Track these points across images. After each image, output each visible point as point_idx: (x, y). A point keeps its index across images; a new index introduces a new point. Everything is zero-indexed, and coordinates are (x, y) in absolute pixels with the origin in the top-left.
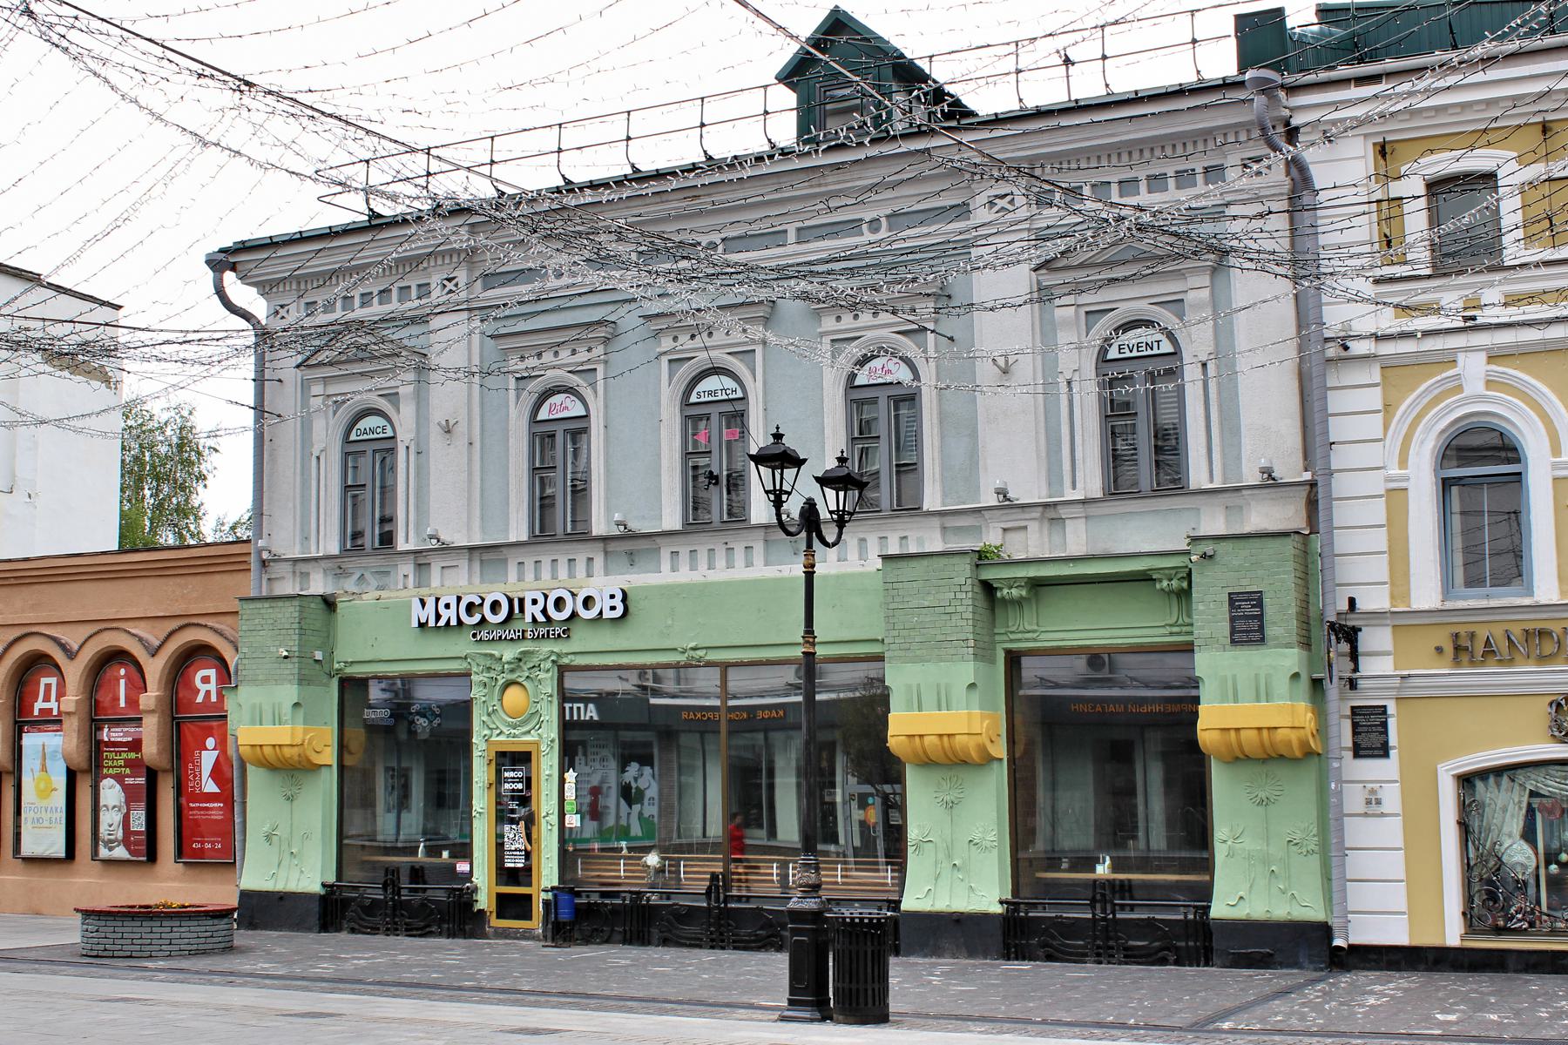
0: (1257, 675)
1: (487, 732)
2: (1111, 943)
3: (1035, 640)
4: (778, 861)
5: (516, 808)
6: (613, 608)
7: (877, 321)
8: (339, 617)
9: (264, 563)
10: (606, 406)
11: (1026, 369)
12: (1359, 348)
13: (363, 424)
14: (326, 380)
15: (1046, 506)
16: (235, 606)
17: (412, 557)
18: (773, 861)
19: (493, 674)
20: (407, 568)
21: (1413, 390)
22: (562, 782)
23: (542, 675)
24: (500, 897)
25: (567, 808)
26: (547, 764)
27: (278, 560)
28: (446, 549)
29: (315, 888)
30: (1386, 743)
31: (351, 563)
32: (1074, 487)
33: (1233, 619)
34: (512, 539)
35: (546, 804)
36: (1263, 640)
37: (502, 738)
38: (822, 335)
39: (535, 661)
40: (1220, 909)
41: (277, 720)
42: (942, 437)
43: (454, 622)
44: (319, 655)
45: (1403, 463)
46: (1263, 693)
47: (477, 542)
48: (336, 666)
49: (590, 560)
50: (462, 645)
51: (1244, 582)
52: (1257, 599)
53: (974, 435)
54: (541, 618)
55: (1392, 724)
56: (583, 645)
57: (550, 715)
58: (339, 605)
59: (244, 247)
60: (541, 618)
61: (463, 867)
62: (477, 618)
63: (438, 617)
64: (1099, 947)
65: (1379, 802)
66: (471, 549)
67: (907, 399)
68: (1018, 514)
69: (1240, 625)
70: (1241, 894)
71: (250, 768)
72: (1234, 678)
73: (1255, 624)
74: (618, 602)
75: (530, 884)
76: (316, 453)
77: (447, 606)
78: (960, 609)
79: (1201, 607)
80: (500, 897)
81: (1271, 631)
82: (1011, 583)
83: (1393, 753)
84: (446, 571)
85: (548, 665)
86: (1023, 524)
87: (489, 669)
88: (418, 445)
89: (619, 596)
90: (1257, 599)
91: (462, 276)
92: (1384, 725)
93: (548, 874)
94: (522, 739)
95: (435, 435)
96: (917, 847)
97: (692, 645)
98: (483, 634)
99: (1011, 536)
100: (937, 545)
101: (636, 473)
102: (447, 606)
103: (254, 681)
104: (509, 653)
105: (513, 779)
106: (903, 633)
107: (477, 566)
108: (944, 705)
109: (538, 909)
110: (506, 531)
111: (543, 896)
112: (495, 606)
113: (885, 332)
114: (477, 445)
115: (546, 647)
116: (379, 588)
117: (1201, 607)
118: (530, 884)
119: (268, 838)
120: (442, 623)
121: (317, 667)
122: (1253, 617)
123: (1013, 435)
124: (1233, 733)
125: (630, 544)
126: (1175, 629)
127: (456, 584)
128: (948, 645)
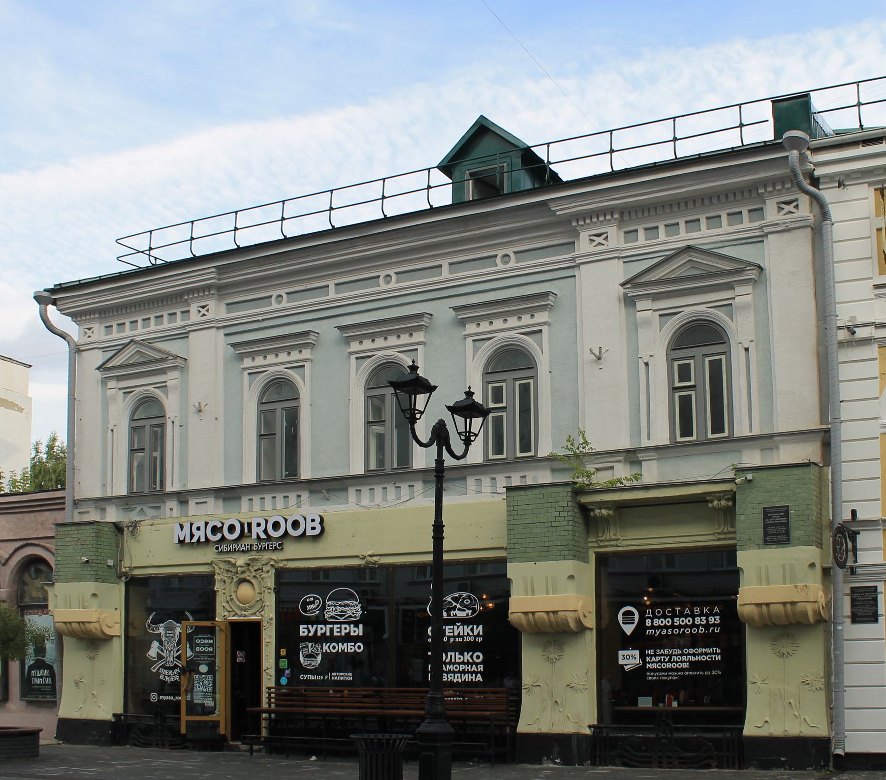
6: (313, 528)
12: (861, 333)
14: (119, 378)
19: (230, 574)
20: (173, 504)
23: (264, 575)
29: (109, 717)
30: (876, 612)
32: (649, 439)
33: (766, 526)
34: (353, 472)
36: (788, 540)
38: (466, 337)
39: (258, 565)
43: (203, 539)
47: (221, 483)
48: (124, 570)
51: (775, 499)
54: (263, 536)
56: (297, 555)
57: (270, 600)
60: (263, 536)
62: (219, 536)
63: (192, 536)
70: (767, 719)
72: (767, 567)
73: (783, 529)
76: (110, 428)
79: (742, 518)
81: (795, 534)
82: (602, 505)
89: (318, 520)
92: (875, 600)
97: (370, 553)
98: (223, 547)
102: (198, 529)
106: (523, 541)
108: (764, 580)
110: (241, 478)
113: (512, 333)
115: (266, 556)
120: (195, 540)
122: (781, 524)
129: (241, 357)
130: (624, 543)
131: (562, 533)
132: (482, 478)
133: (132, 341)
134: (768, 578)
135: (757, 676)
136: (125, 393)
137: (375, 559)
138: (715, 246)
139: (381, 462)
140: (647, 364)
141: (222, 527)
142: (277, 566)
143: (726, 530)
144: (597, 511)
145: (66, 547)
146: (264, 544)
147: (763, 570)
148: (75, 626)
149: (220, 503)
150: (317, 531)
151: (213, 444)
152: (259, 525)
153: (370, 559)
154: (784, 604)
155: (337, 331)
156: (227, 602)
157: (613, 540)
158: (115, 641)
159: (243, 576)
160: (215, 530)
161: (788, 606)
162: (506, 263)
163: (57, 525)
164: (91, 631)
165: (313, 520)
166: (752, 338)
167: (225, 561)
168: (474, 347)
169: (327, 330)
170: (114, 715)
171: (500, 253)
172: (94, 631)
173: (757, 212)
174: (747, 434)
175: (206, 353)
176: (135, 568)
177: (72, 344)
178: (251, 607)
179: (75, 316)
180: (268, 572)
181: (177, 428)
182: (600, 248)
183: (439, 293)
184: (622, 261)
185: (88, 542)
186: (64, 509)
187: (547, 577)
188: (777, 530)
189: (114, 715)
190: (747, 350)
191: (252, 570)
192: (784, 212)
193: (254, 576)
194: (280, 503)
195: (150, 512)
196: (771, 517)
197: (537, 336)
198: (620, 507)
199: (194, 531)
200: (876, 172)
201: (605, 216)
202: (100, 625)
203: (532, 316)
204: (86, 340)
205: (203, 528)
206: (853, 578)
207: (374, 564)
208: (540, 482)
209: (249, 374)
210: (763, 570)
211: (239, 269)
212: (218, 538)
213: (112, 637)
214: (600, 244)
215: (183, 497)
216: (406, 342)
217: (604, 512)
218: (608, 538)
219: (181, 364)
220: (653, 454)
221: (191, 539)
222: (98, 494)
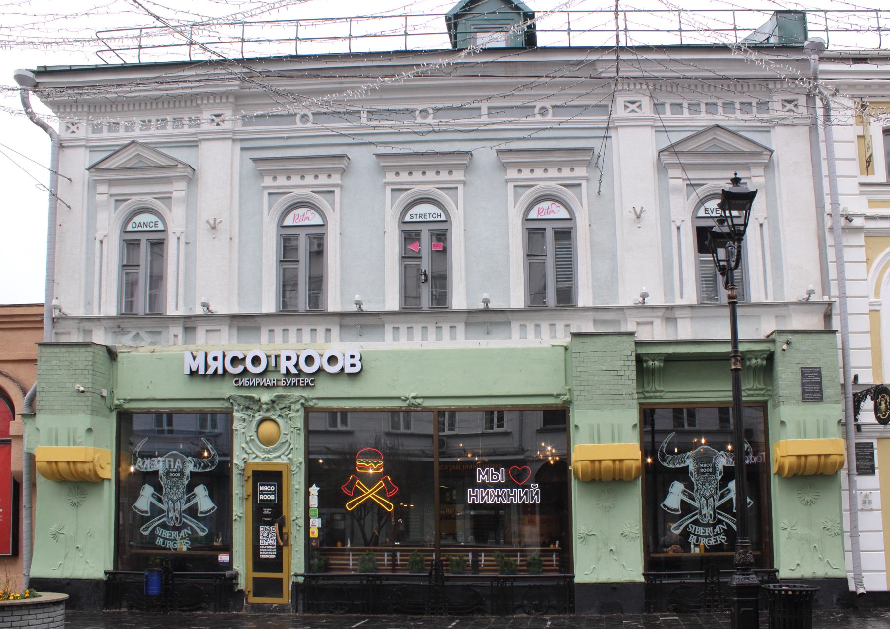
0: (818, 421)
1: (245, 456)
2: (717, 598)
3: (661, 397)
4: (388, 551)
5: (270, 514)
6: (353, 365)
7: (547, 175)
8: (119, 364)
9: (54, 321)
10: (341, 219)
11: (652, 216)
12: (857, 222)
13: (139, 219)
14: (111, 183)
15: (667, 308)
16: (34, 352)
17: (182, 321)
18: (468, 551)
19: (249, 412)
20: (179, 330)
21: (881, 251)
22: (307, 494)
23: (292, 414)
24: (255, 580)
25: (311, 513)
26: (297, 481)
27: (65, 318)
28: (210, 317)
29: (100, 574)
30: (873, 465)
31: (125, 324)
32: (682, 297)
33: (803, 385)
34: (265, 310)
35: (294, 511)
36: (822, 398)
37: (257, 460)
38: (507, 181)
39: (286, 403)
40: (580, 576)
41: (72, 441)
42: (592, 259)
43: (220, 371)
44: (105, 393)
45: (877, 295)
46: (822, 432)
47: (236, 311)
48: (117, 402)
49: (328, 330)
50: (227, 389)
51: (809, 361)
52: (818, 372)
53: (614, 257)
55: (875, 452)
56: (326, 393)
57: (299, 443)
58: (120, 356)
59: (44, 72)
60: (294, 371)
61: (224, 558)
62: (240, 369)
63: (206, 367)
64: (709, 601)
65: (870, 502)
66: (234, 317)
67: (565, 235)
68: (649, 313)
69: (808, 388)
70: (797, 562)
71: (40, 480)
72: (805, 421)
73: (817, 388)
74: (356, 360)
75: (281, 571)
76: (99, 236)
77: (215, 359)
78: (627, 372)
79: (784, 376)
80: (255, 580)
81: (826, 392)
82: (654, 357)
83: (876, 471)
84: (211, 334)
85: (298, 406)
86: (650, 320)
87: (247, 408)
88: (187, 237)
89: (358, 357)
90: (818, 372)
91: (228, 114)
92: (872, 454)
93: (296, 564)
94: (277, 459)
95: (202, 230)
96: (585, 538)
97: (414, 394)
98: (245, 381)
99: (641, 328)
100: (591, 329)
101: (364, 267)
102: (215, 359)
103: (51, 410)
104: (266, 397)
105: (267, 492)
106: (589, 388)
107: (235, 332)
109: (288, 588)
110: (260, 306)
111: (293, 579)
112: (256, 360)
113: (553, 184)
114: (236, 240)
115: (296, 393)
116: (152, 344)
117: (784, 376)
118: (281, 571)
119: (55, 536)
120: (210, 371)
121: (103, 402)
122: (816, 383)
123: (638, 263)
124: (803, 458)
125: (361, 320)
126: (751, 392)
127: (221, 345)
128: (620, 397)
129: (262, 174)
130: (667, 395)
131: (627, 382)
132: (528, 324)
133: (133, 142)
134: (799, 433)
135: (786, 521)
136: (116, 200)
137: (419, 401)
138: (741, 129)
139: (130, 305)
140: (679, 228)
141: (244, 359)
142: (307, 404)
143: (755, 387)
144: (650, 363)
145: (52, 372)
146: (294, 380)
147: (802, 425)
148: (62, 466)
149: (235, 332)
150: (356, 369)
151: (222, 264)
152: (289, 358)
153: (413, 401)
154: (819, 456)
155: (251, 164)
156: (247, 443)
157: (658, 392)
158: (106, 483)
159: (268, 414)
160: (235, 361)
161: (617, 463)
162: (425, 117)
163: (41, 345)
164: (83, 473)
165: (352, 357)
166: (765, 215)
167: (246, 397)
168: (515, 192)
169: (485, 155)
170: (106, 573)
171: (539, 105)
172: (87, 472)
173: (763, 105)
174: (764, 301)
175: (220, 165)
176: (131, 400)
177: (55, 137)
178: (276, 449)
179: (56, 106)
180: (297, 411)
181: (182, 245)
182: (633, 115)
183: (481, 135)
184: (654, 130)
185: (81, 367)
186: (42, 328)
187: (612, 425)
188: (812, 388)
189: (106, 573)
190: (761, 225)
191: (278, 408)
192: (629, 110)
193: (280, 415)
194: (306, 336)
195: (147, 338)
196: (807, 377)
197: (577, 189)
198: (669, 359)
199: (210, 361)
200: (858, 87)
201: (228, 97)
202: (94, 466)
203: (572, 170)
204: (68, 135)
205: (220, 358)
206: (860, 434)
207: (417, 406)
208: (584, 330)
209: (270, 194)
210: (802, 425)
211: (257, 81)
212: (238, 372)
213: (103, 480)
214: (633, 111)
215: (189, 324)
216: (404, 180)
217: (657, 363)
218: (653, 389)
219: (191, 176)
220: (687, 313)
221: (206, 370)
222: (81, 313)
